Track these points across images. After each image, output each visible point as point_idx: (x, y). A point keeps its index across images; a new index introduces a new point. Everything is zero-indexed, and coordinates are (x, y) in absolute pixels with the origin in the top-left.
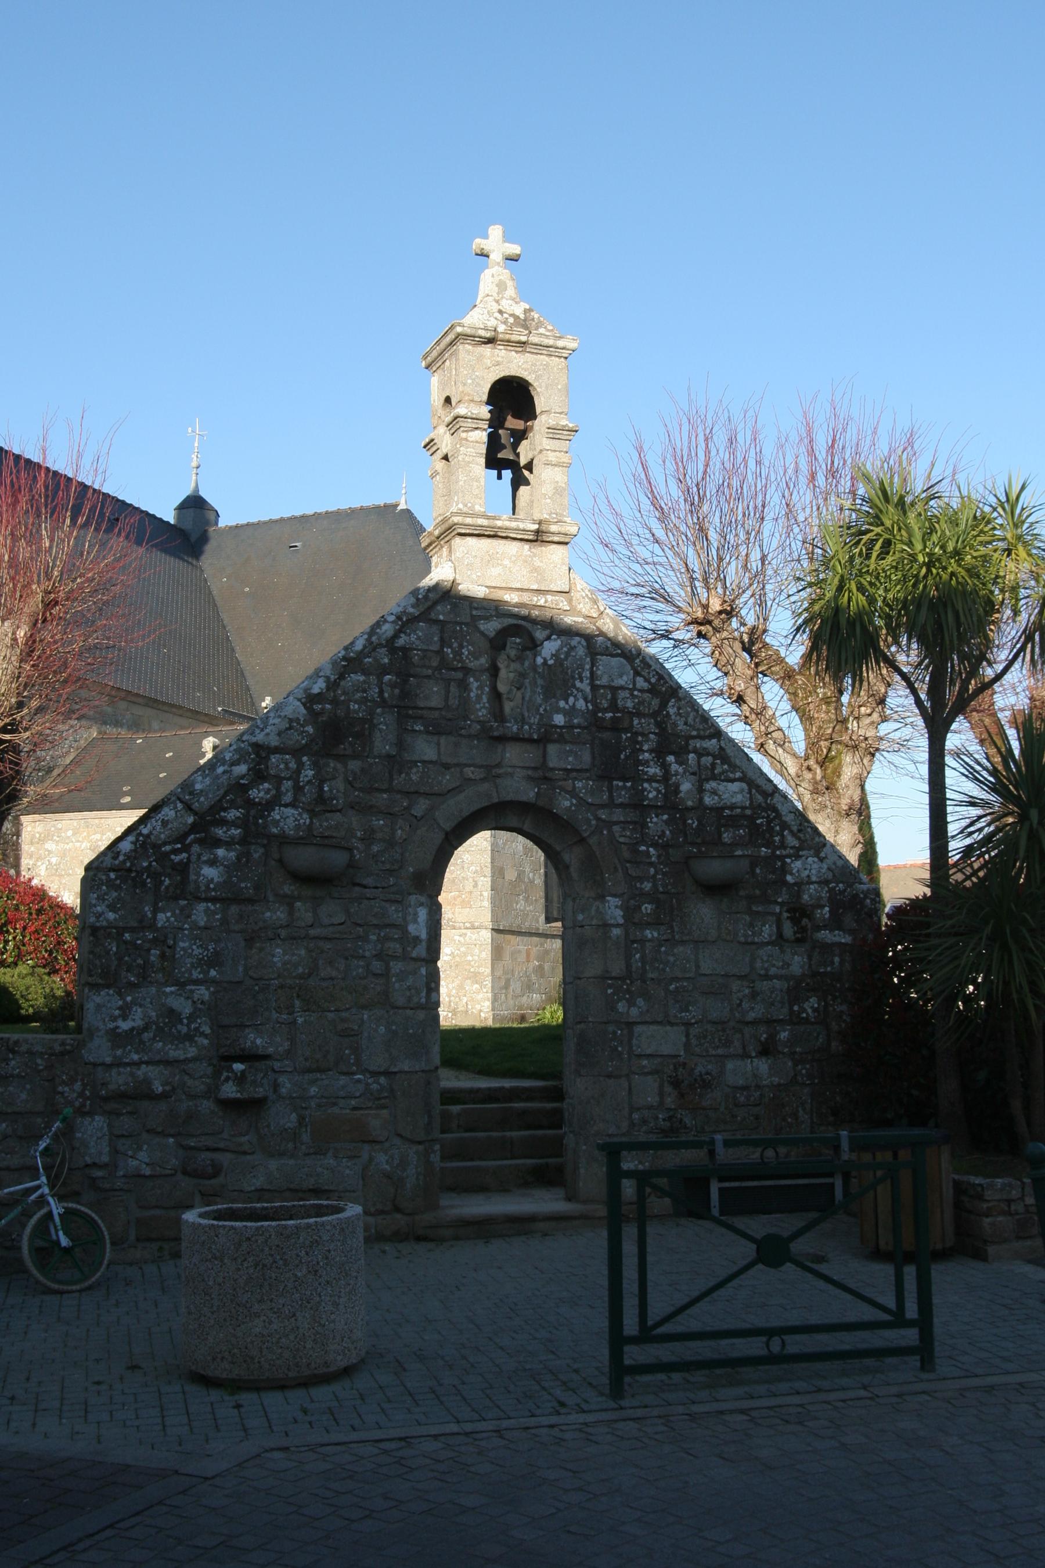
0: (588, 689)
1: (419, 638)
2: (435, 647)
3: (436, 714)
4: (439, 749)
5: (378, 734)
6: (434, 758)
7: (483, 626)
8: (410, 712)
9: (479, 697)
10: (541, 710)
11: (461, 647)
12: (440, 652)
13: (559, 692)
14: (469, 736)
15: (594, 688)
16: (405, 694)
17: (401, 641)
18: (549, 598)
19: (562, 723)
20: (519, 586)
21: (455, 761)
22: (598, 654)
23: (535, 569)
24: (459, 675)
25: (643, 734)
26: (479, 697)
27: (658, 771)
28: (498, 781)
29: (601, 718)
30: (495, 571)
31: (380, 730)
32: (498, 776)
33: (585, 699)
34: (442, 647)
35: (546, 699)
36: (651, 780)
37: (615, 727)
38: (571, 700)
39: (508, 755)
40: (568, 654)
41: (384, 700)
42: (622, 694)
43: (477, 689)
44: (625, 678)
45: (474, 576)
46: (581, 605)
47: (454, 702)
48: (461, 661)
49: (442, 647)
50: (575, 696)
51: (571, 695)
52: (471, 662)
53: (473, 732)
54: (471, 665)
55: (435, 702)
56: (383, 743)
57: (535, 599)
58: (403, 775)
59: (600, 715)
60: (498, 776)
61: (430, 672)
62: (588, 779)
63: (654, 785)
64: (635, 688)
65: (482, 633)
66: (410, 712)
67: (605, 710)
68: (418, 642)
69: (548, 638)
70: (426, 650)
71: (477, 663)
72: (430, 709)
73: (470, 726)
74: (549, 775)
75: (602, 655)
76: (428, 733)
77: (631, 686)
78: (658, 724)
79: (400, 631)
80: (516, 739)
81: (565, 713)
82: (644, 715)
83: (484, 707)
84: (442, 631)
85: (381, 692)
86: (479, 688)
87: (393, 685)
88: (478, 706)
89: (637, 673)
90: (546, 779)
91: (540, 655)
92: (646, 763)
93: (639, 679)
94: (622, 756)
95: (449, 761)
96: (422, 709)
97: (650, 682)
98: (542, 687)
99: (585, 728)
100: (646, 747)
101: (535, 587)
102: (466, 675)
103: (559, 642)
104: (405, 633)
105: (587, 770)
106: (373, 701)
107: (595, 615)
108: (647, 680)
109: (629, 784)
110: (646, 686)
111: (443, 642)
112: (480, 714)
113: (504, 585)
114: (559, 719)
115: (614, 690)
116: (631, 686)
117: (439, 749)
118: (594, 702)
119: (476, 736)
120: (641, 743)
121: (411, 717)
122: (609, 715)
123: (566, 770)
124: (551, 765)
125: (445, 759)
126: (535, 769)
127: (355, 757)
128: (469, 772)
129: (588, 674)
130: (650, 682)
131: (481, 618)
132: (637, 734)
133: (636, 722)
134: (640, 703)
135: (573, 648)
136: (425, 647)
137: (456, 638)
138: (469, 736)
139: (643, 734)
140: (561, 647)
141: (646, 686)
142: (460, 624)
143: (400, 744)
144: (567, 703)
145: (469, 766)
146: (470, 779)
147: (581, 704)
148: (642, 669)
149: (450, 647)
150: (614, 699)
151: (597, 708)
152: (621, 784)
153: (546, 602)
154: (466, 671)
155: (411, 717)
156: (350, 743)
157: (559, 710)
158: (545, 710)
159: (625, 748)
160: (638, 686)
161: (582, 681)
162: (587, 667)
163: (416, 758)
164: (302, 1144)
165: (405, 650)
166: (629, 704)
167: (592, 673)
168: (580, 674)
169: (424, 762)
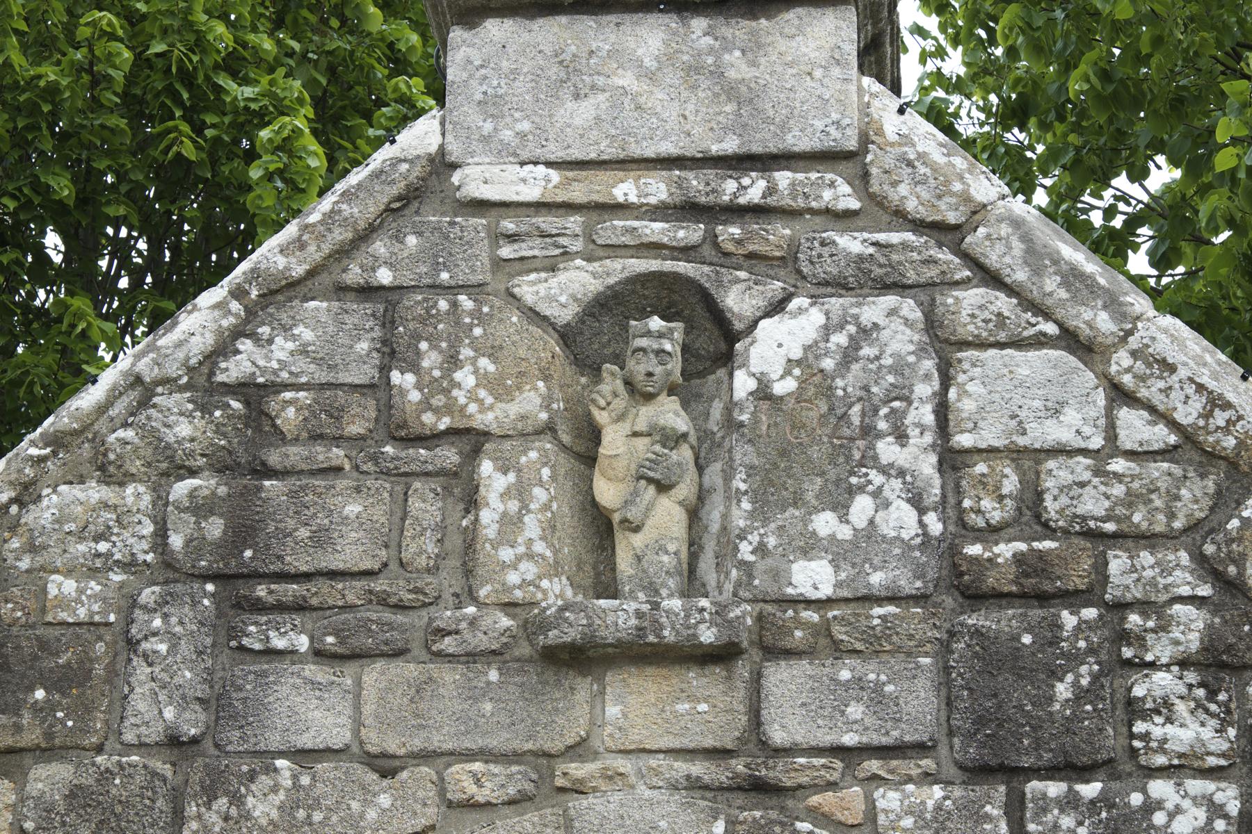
0: (927, 466)
1: (303, 351)
2: (363, 373)
3: (352, 592)
4: (357, 707)
5: (142, 671)
6: (340, 736)
7: (530, 288)
8: (261, 591)
9: (511, 524)
10: (745, 551)
11: (453, 361)
12: (379, 388)
13: (812, 487)
14: (471, 657)
15: (952, 460)
16: (244, 530)
17: (234, 369)
18: (783, 178)
19: (826, 591)
20: (668, 148)
21: (417, 744)
22: (964, 344)
23: (731, 91)
24: (449, 456)
25: (1144, 606)
26: (511, 524)
27: (1207, 733)
28: (577, 804)
29: (975, 560)
30: (581, 113)
31: (148, 659)
32: (578, 789)
33: (917, 501)
34: (385, 370)
35: (761, 513)
36: (1184, 767)
37: (1037, 588)
38: (862, 507)
39: (613, 711)
40: (849, 356)
41: (167, 562)
42: (1057, 474)
43: (505, 495)
44: (1071, 416)
45: (507, 135)
46: (903, 189)
47: (422, 548)
48: (449, 408)
49: (385, 370)
50: (877, 494)
51: (861, 489)
52: (483, 409)
53: (480, 641)
54: (485, 420)
55: (351, 552)
56: (156, 703)
57: (731, 186)
58: (223, 802)
59: (974, 550)
60: (578, 789)
61: (337, 454)
62: (928, 778)
63: (1196, 786)
64: (1112, 446)
65: (533, 315)
66: (261, 591)
67: (992, 532)
68: (301, 364)
69: (777, 307)
70: (323, 387)
71: (514, 409)
72: (333, 575)
73: (473, 622)
74: (777, 772)
75: (982, 345)
76: (319, 654)
77: (1097, 442)
78: (1206, 567)
79: (238, 333)
80: (645, 653)
81: (838, 553)
82: (1148, 539)
83: (530, 556)
84: (388, 322)
85: (161, 534)
86: (520, 491)
87: (200, 508)
88: (506, 554)
89: (1120, 395)
90: (759, 788)
91: (744, 365)
92: (1164, 708)
93: (1125, 415)
94: (1063, 690)
95: (392, 746)
96: (307, 577)
97: (1173, 425)
98: (751, 470)
99: (919, 599)
100: (1160, 650)
101: (730, 145)
102: (473, 456)
103: (816, 317)
104: (253, 336)
105: (921, 748)
106: (130, 565)
107: (952, 218)
108: (1158, 415)
109: (1090, 790)
110: (1161, 436)
111: (392, 353)
112: (513, 578)
113: (610, 153)
114: (813, 577)
115: (1029, 458)
116: (1097, 442)
117: (357, 707)
118: (951, 506)
119: (530, 660)
120: (1138, 640)
121: (259, 607)
122: (1005, 550)
123: (838, 751)
124: (778, 736)
125: (375, 741)
126: (718, 754)
127: (48, 752)
128: (464, 779)
129: (927, 414)
130: (1173, 425)
131: (524, 264)
132: (1121, 607)
133: (1117, 564)
134: (1132, 499)
135: (866, 333)
136: (323, 376)
137: (433, 340)
138: (471, 657)
139: (1144, 606)
140: (827, 330)
141: (1161, 436)
142: (451, 290)
143: (219, 703)
144: (844, 519)
145: (469, 756)
146: (470, 805)
147: (901, 519)
148: (1142, 378)
149: (414, 367)
150: (1031, 498)
151: (962, 528)
152: (1055, 789)
153: (771, 190)
154: (473, 440)
155: (259, 607)
156: (36, 708)
157: (810, 547)
158: (761, 549)
159: (1075, 659)
160: (1127, 440)
161: (901, 437)
162: (924, 390)
163: (274, 741)
164: (134, 167)
165: (255, 393)
166: (1092, 504)
167: (942, 410)
168: (897, 418)
169: (304, 756)
